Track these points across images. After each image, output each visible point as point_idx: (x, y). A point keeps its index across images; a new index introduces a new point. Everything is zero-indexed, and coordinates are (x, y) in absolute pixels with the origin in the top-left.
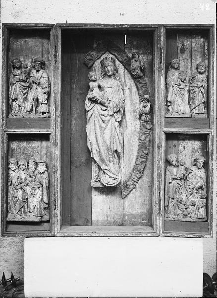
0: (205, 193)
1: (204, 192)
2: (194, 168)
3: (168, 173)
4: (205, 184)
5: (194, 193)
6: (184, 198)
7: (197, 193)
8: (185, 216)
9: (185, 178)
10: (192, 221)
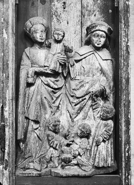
0: (111, 106)
1: (110, 105)
2: (87, 49)
3: (25, 61)
4: (112, 84)
5: (86, 108)
6: (64, 120)
7: (94, 107)
8: (66, 162)
9: (63, 71)
10: (83, 173)
